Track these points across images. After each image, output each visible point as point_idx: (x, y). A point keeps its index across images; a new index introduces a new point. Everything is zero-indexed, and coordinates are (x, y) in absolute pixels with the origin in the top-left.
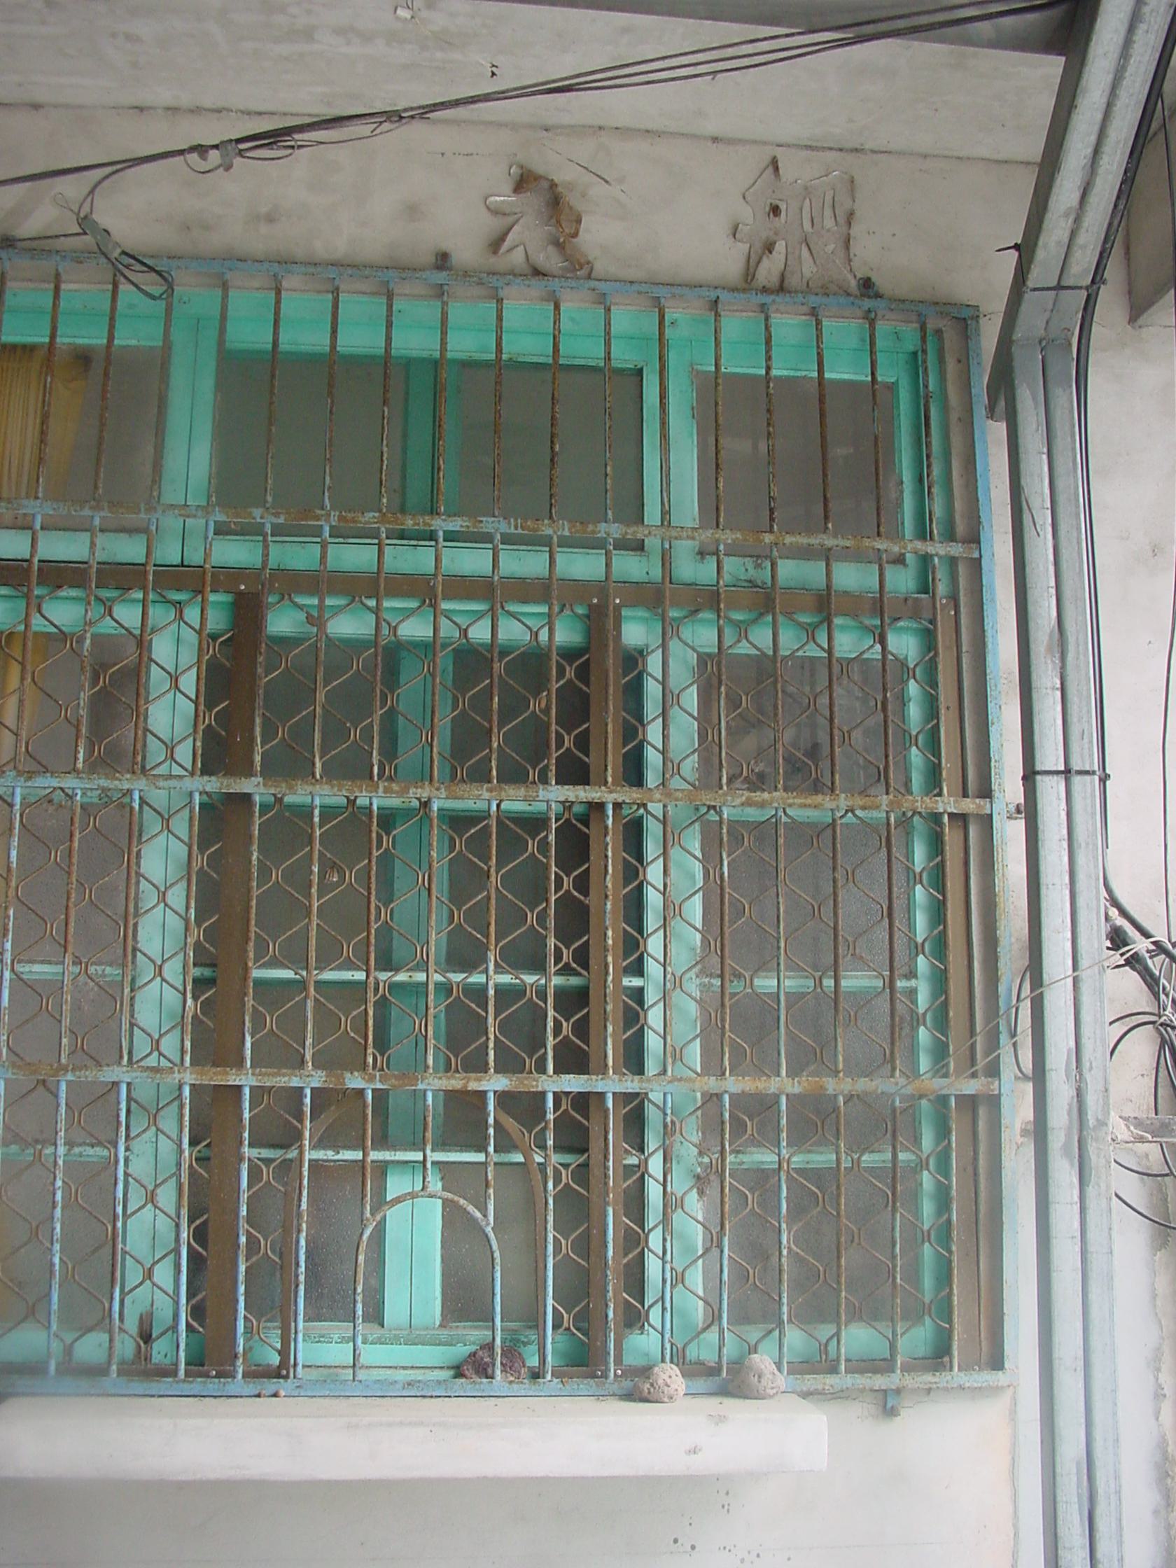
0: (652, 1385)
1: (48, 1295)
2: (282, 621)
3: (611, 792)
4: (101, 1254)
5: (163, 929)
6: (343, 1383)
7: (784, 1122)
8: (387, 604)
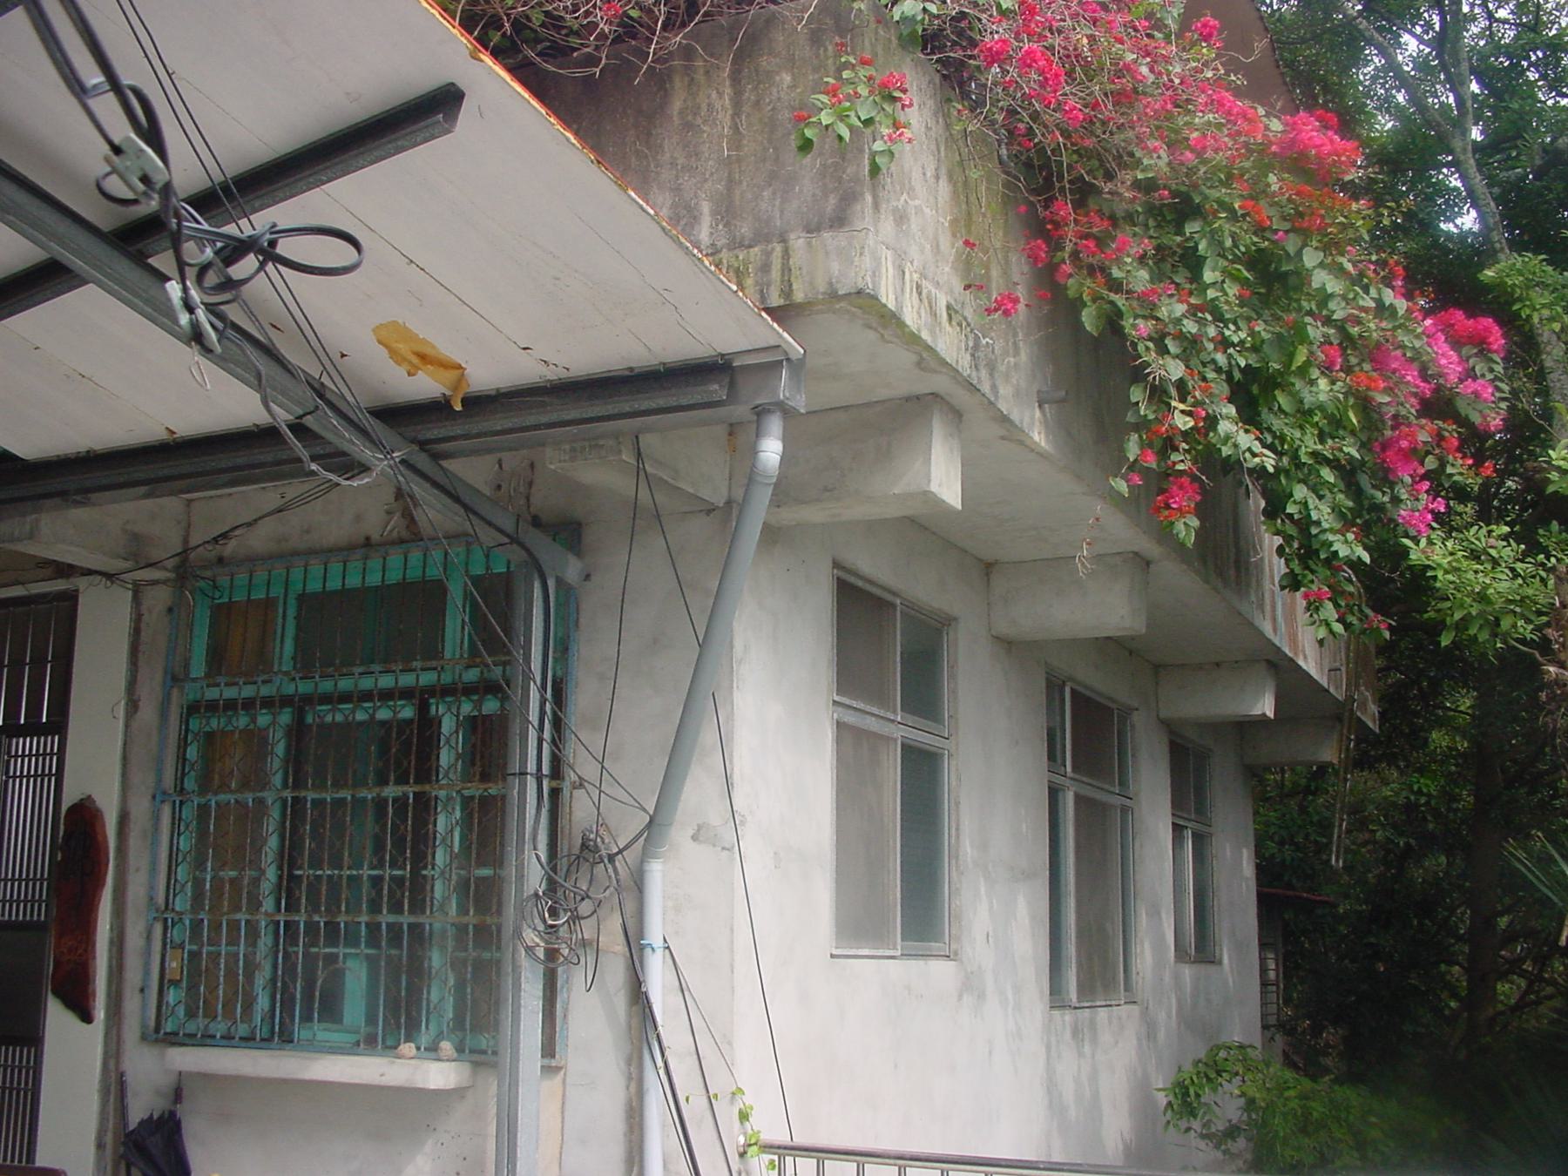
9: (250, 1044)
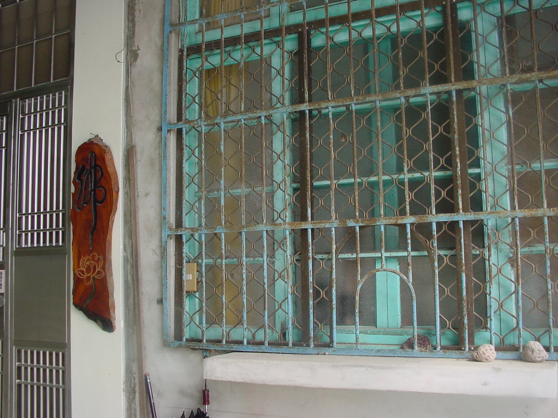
0: (478, 353)
1: (222, 312)
2: (318, 41)
3: (453, 85)
4: (261, 298)
5: (282, 171)
6: (352, 350)
7: (547, 229)
8: (330, 29)
9: (284, 349)
